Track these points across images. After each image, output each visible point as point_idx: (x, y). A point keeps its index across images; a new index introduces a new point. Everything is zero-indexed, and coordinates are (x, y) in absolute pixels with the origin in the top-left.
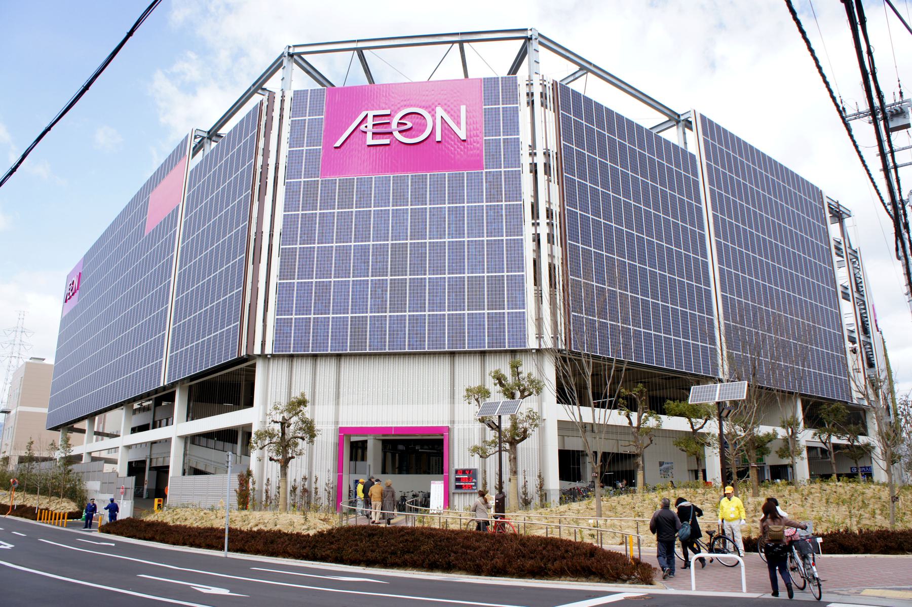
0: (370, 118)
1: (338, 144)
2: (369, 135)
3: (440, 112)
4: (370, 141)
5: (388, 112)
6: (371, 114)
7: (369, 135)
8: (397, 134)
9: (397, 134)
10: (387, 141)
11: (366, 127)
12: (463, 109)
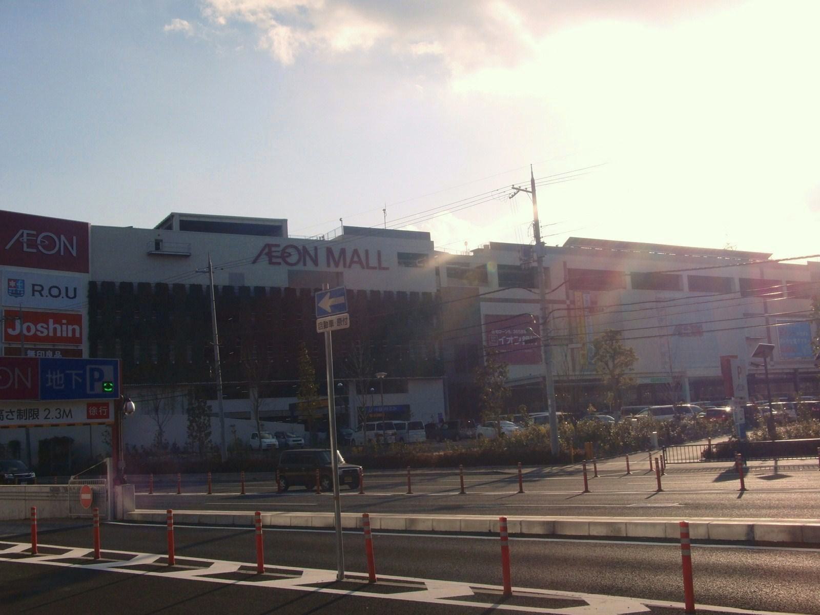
0: (25, 235)
1: (8, 247)
2: (25, 245)
3: (17, 371)
4: (25, 249)
5: (34, 232)
6: (26, 232)
7: (25, 245)
8: (40, 248)
9: (40, 248)
10: (34, 251)
11: (23, 239)
12: (75, 238)
